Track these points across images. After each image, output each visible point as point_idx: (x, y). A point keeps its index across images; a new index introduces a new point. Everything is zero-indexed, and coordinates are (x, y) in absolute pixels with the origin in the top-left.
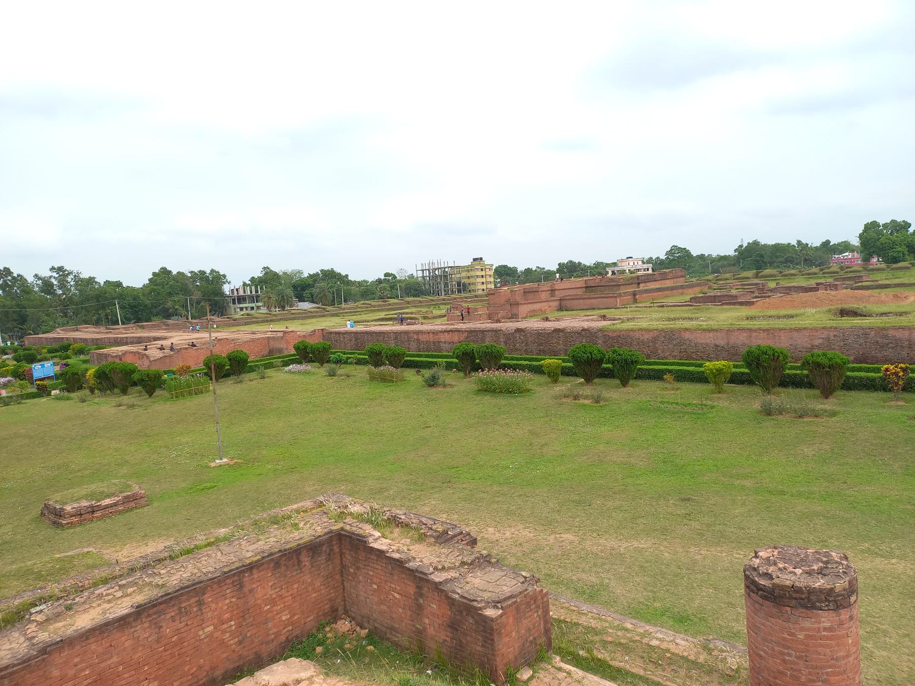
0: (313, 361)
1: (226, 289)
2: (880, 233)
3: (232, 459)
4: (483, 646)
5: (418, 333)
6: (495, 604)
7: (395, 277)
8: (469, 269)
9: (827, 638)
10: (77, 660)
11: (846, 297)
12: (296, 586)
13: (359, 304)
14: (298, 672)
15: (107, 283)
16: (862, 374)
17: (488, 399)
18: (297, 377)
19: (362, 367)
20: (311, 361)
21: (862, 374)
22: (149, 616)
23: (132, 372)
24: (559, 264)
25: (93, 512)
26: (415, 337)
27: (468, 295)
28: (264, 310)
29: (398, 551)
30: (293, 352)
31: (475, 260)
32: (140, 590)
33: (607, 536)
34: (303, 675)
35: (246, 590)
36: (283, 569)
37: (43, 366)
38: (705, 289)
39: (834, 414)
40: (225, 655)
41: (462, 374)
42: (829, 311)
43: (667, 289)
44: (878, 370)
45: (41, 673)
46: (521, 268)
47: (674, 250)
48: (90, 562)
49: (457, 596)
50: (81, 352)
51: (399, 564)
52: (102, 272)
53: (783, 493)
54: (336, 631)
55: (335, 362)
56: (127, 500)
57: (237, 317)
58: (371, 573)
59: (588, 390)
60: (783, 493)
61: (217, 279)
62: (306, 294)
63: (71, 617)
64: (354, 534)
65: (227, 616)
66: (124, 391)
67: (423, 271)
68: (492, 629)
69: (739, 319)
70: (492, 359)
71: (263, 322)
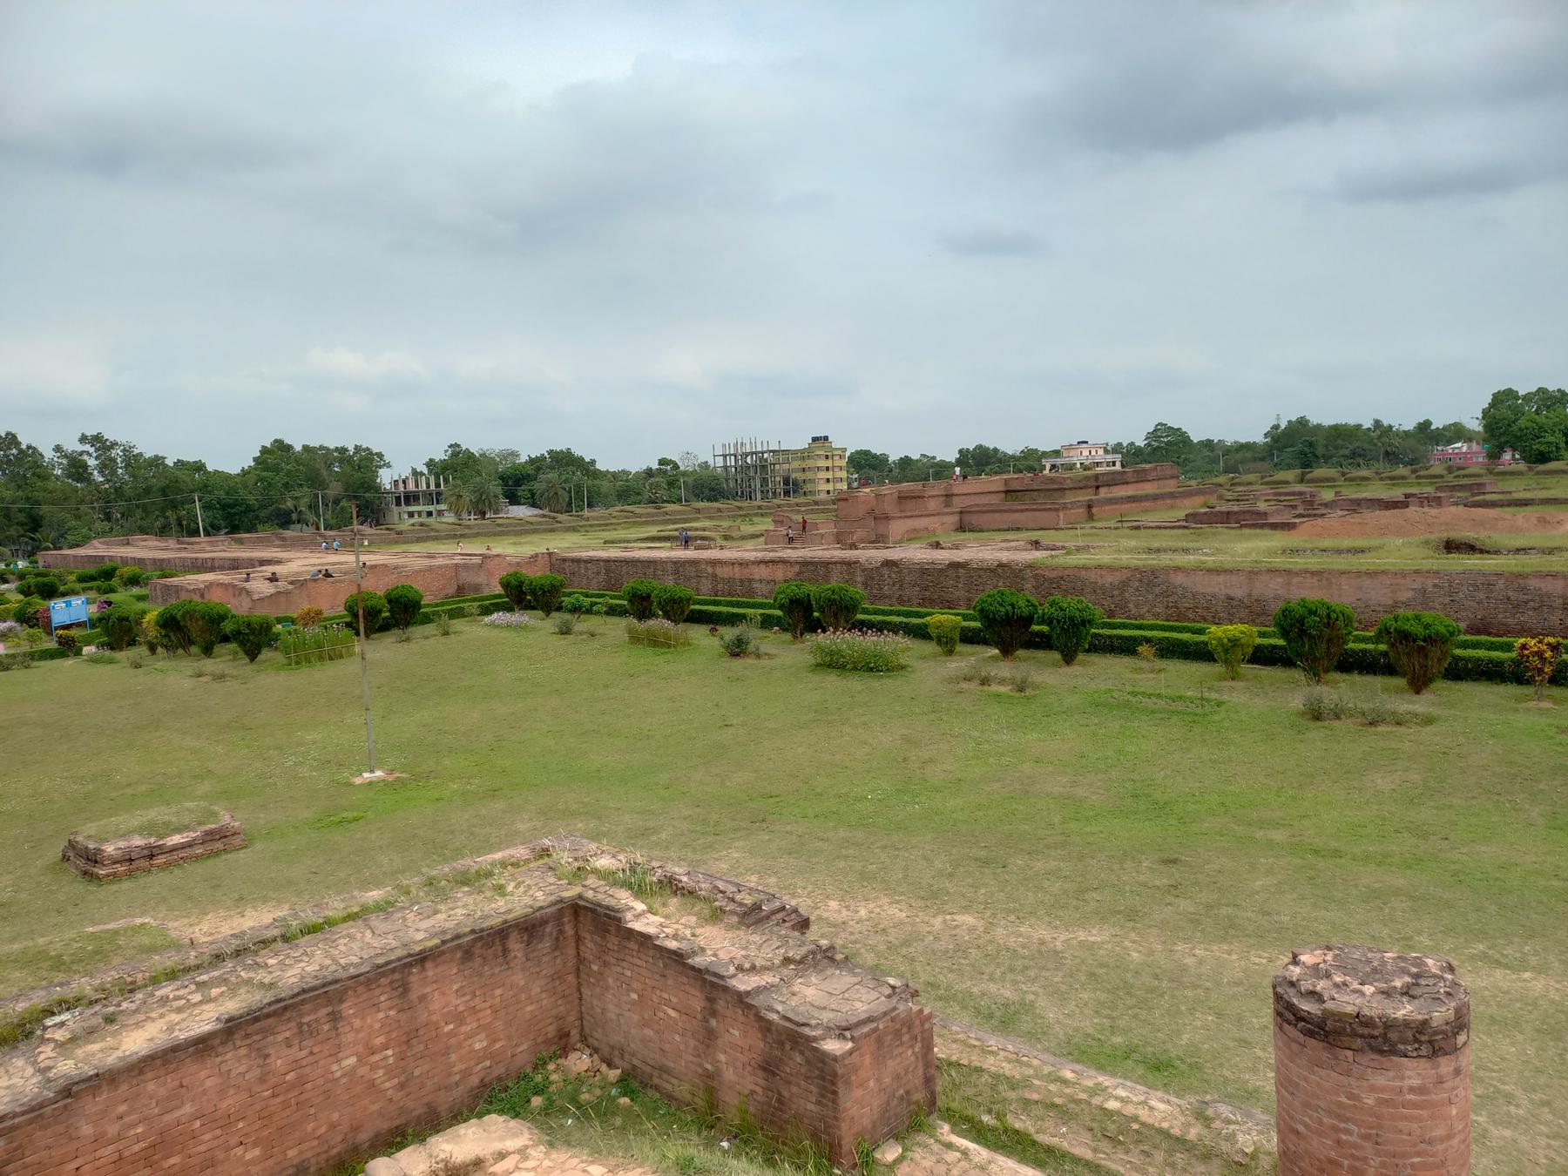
0: (533, 608)
1: (386, 478)
2: (1518, 412)
3: (391, 772)
4: (818, 1103)
5: (714, 563)
6: (842, 1031)
7: (676, 467)
8: (804, 455)
9: (1415, 1105)
10: (123, 1108)
12: (498, 992)
13: (614, 511)
14: (502, 1139)
15: (180, 464)
16: (1481, 653)
17: (832, 680)
18: (504, 634)
20: (530, 607)
21: (1481, 653)
22: (247, 1036)
23: (223, 617)
24: (960, 451)
25: (152, 856)
26: (710, 570)
27: (802, 500)
28: (449, 518)
29: (675, 937)
30: (499, 590)
31: (815, 439)
33: (1033, 921)
34: (510, 1145)
35: (413, 996)
37: (68, 604)
38: (1213, 500)
39: (1429, 721)
40: (375, 1107)
41: (788, 636)
42: (1427, 543)
43: (1155, 498)
44: (1508, 647)
45: (60, 1129)
47: (1160, 431)
49: (775, 1017)
50: (134, 581)
51: (677, 959)
52: (167, 438)
53: (1337, 853)
56: (210, 836)
58: (629, 973)
60: (1337, 853)
62: (522, 491)
63: (114, 1034)
64: (600, 905)
65: (380, 1040)
66: (208, 651)
67: (725, 456)
68: (835, 1074)
69: (1272, 553)
70: (841, 613)
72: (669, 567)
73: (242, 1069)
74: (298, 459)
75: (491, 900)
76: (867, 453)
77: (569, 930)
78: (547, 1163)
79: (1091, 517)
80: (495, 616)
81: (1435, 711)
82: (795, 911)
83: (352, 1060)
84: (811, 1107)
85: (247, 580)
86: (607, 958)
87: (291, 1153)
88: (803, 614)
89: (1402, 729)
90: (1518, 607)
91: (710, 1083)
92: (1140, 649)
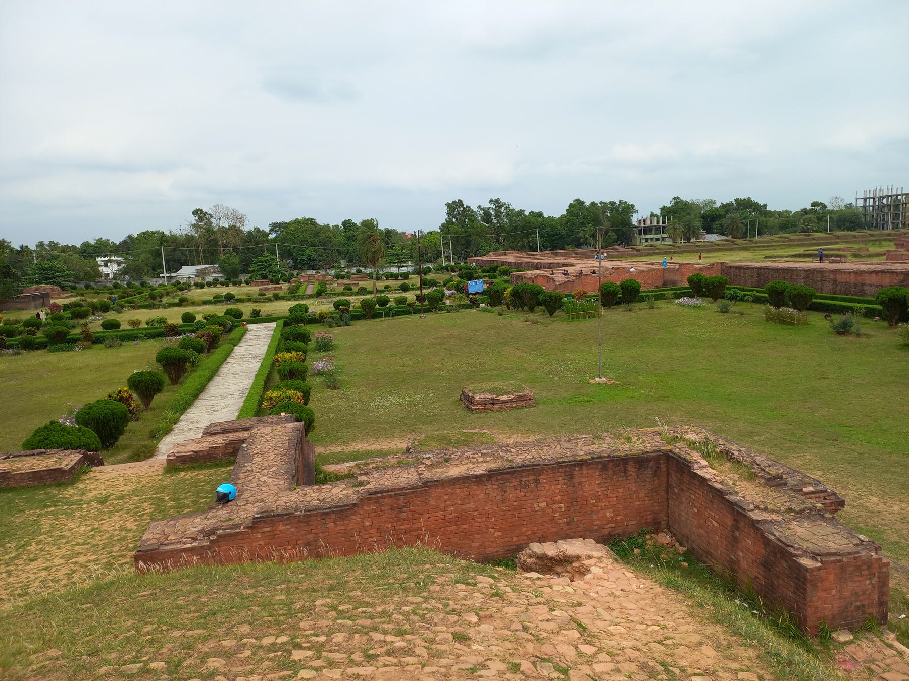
0: (707, 296)
1: (635, 219)
3: (610, 379)
4: (794, 593)
5: (835, 272)
6: (814, 556)
7: (825, 207)
10: (446, 497)
12: (621, 490)
13: (775, 237)
14: (592, 551)
15: (532, 213)
18: (686, 310)
19: (758, 305)
20: (704, 295)
22: (498, 480)
23: (539, 292)
25: (494, 404)
26: (832, 276)
28: (669, 242)
29: (721, 482)
30: (687, 285)
32: (495, 460)
34: (594, 554)
35: (575, 481)
36: (610, 472)
40: (554, 530)
41: (886, 324)
45: (423, 499)
48: (485, 440)
49: (773, 538)
50: (505, 273)
51: (719, 495)
52: (524, 202)
54: (656, 542)
55: (729, 299)
56: (520, 399)
57: (640, 247)
58: (693, 497)
61: (627, 209)
62: (716, 225)
63: (447, 467)
65: (558, 498)
66: (532, 310)
67: (865, 199)
68: (806, 579)
71: (665, 253)
72: (803, 275)
73: (495, 494)
74: (587, 209)
75: (623, 444)
77: (663, 467)
78: (610, 567)
83: (544, 504)
84: (789, 593)
85: (553, 274)
87: (514, 539)
91: (733, 566)
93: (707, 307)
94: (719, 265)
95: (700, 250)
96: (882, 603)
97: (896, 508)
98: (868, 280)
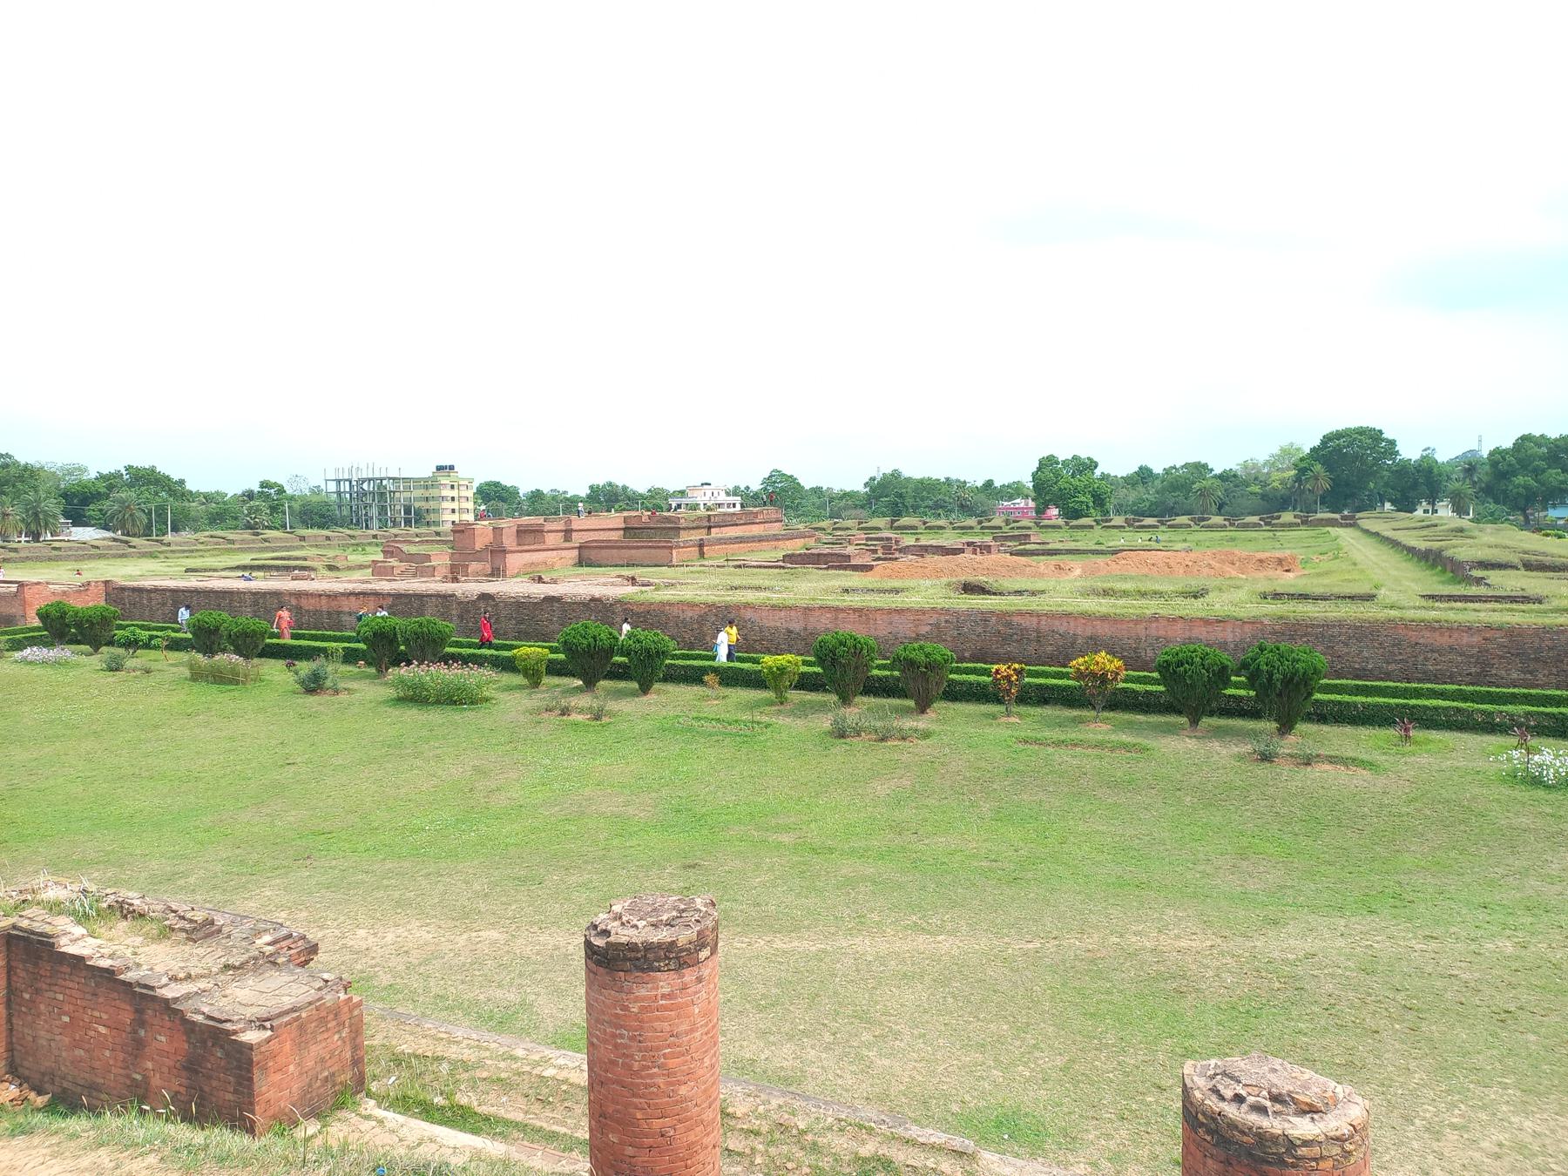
0: (79, 643)
2: (1057, 475)
4: (236, 1092)
5: (299, 595)
6: (261, 1023)
7: (281, 491)
8: (428, 484)
9: (666, 1008)
11: (995, 566)
13: (201, 536)
16: (972, 678)
17: (412, 714)
18: (38, 671)
21: (972, 678)
24: (591, 487)
26: (294, 602)
27: (423, 530)
29: (111, 956)
30: (37, 623)
31: (439, 468)
33: (554, 929)
38: (811, 542)
39: (926, 735)
41: (373, 670)
42: (949, 585)
43: (760, 539)
44: (986, 672)
46: (525, 489)
47: (774, 478)
51: (108, 976)
53: (831, 850)
55: (121, 645)
58: (60, 997)
59: (584, 701)
60: (831, 850)
62: (92, 510)
64: (33, 933)
69: (826, 591)
70: (428, 647)
76: (497, 484)
79: (702, 554)
80: (28, 650)
81: (933, 727)
82: (303, 938)
84: (229, 1097)
86: (39, 985)
88: (383, 650)
89: (907, 743)
90: (1006, 639)
92: (706, 678)
93: (82, 663)
94: (102, 587)
95: (57, 556)
96: (357, 1062)
97: (390, 937)
98: (347, 605)
